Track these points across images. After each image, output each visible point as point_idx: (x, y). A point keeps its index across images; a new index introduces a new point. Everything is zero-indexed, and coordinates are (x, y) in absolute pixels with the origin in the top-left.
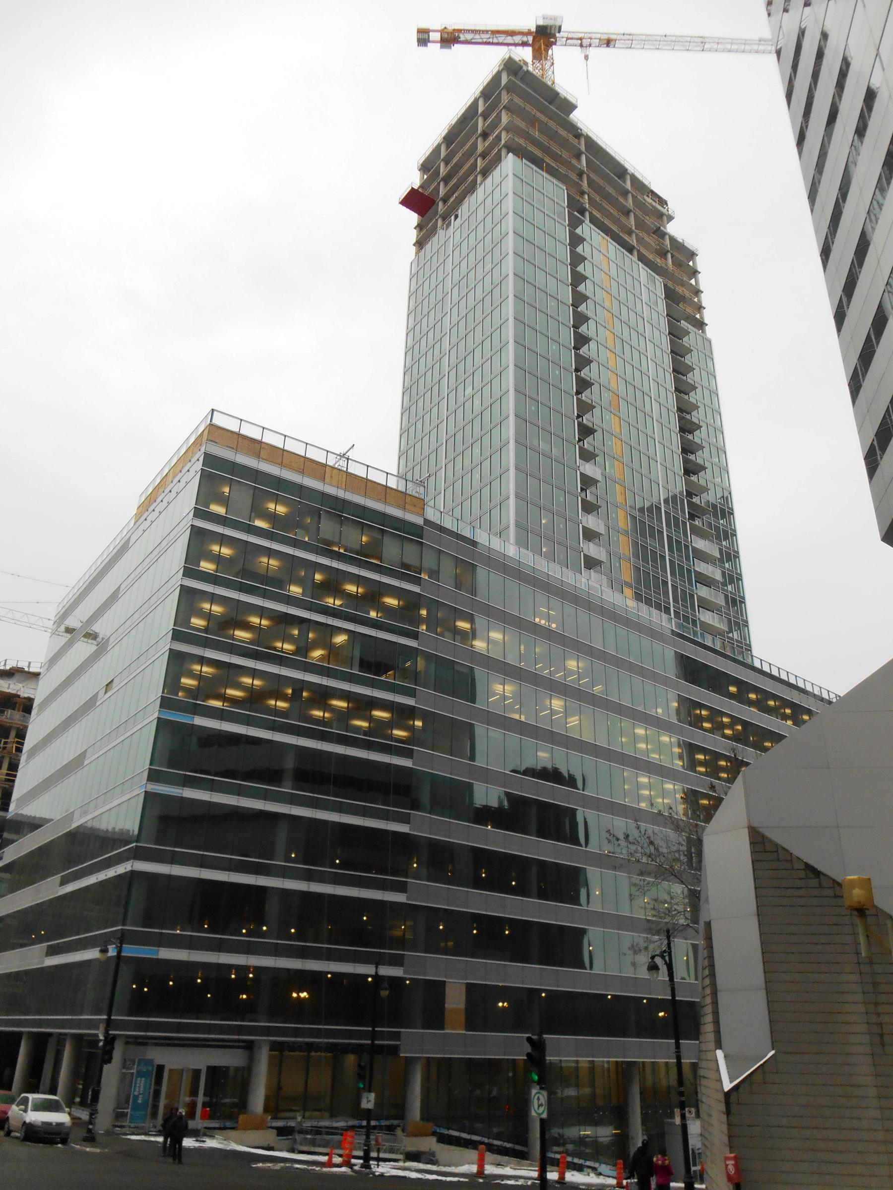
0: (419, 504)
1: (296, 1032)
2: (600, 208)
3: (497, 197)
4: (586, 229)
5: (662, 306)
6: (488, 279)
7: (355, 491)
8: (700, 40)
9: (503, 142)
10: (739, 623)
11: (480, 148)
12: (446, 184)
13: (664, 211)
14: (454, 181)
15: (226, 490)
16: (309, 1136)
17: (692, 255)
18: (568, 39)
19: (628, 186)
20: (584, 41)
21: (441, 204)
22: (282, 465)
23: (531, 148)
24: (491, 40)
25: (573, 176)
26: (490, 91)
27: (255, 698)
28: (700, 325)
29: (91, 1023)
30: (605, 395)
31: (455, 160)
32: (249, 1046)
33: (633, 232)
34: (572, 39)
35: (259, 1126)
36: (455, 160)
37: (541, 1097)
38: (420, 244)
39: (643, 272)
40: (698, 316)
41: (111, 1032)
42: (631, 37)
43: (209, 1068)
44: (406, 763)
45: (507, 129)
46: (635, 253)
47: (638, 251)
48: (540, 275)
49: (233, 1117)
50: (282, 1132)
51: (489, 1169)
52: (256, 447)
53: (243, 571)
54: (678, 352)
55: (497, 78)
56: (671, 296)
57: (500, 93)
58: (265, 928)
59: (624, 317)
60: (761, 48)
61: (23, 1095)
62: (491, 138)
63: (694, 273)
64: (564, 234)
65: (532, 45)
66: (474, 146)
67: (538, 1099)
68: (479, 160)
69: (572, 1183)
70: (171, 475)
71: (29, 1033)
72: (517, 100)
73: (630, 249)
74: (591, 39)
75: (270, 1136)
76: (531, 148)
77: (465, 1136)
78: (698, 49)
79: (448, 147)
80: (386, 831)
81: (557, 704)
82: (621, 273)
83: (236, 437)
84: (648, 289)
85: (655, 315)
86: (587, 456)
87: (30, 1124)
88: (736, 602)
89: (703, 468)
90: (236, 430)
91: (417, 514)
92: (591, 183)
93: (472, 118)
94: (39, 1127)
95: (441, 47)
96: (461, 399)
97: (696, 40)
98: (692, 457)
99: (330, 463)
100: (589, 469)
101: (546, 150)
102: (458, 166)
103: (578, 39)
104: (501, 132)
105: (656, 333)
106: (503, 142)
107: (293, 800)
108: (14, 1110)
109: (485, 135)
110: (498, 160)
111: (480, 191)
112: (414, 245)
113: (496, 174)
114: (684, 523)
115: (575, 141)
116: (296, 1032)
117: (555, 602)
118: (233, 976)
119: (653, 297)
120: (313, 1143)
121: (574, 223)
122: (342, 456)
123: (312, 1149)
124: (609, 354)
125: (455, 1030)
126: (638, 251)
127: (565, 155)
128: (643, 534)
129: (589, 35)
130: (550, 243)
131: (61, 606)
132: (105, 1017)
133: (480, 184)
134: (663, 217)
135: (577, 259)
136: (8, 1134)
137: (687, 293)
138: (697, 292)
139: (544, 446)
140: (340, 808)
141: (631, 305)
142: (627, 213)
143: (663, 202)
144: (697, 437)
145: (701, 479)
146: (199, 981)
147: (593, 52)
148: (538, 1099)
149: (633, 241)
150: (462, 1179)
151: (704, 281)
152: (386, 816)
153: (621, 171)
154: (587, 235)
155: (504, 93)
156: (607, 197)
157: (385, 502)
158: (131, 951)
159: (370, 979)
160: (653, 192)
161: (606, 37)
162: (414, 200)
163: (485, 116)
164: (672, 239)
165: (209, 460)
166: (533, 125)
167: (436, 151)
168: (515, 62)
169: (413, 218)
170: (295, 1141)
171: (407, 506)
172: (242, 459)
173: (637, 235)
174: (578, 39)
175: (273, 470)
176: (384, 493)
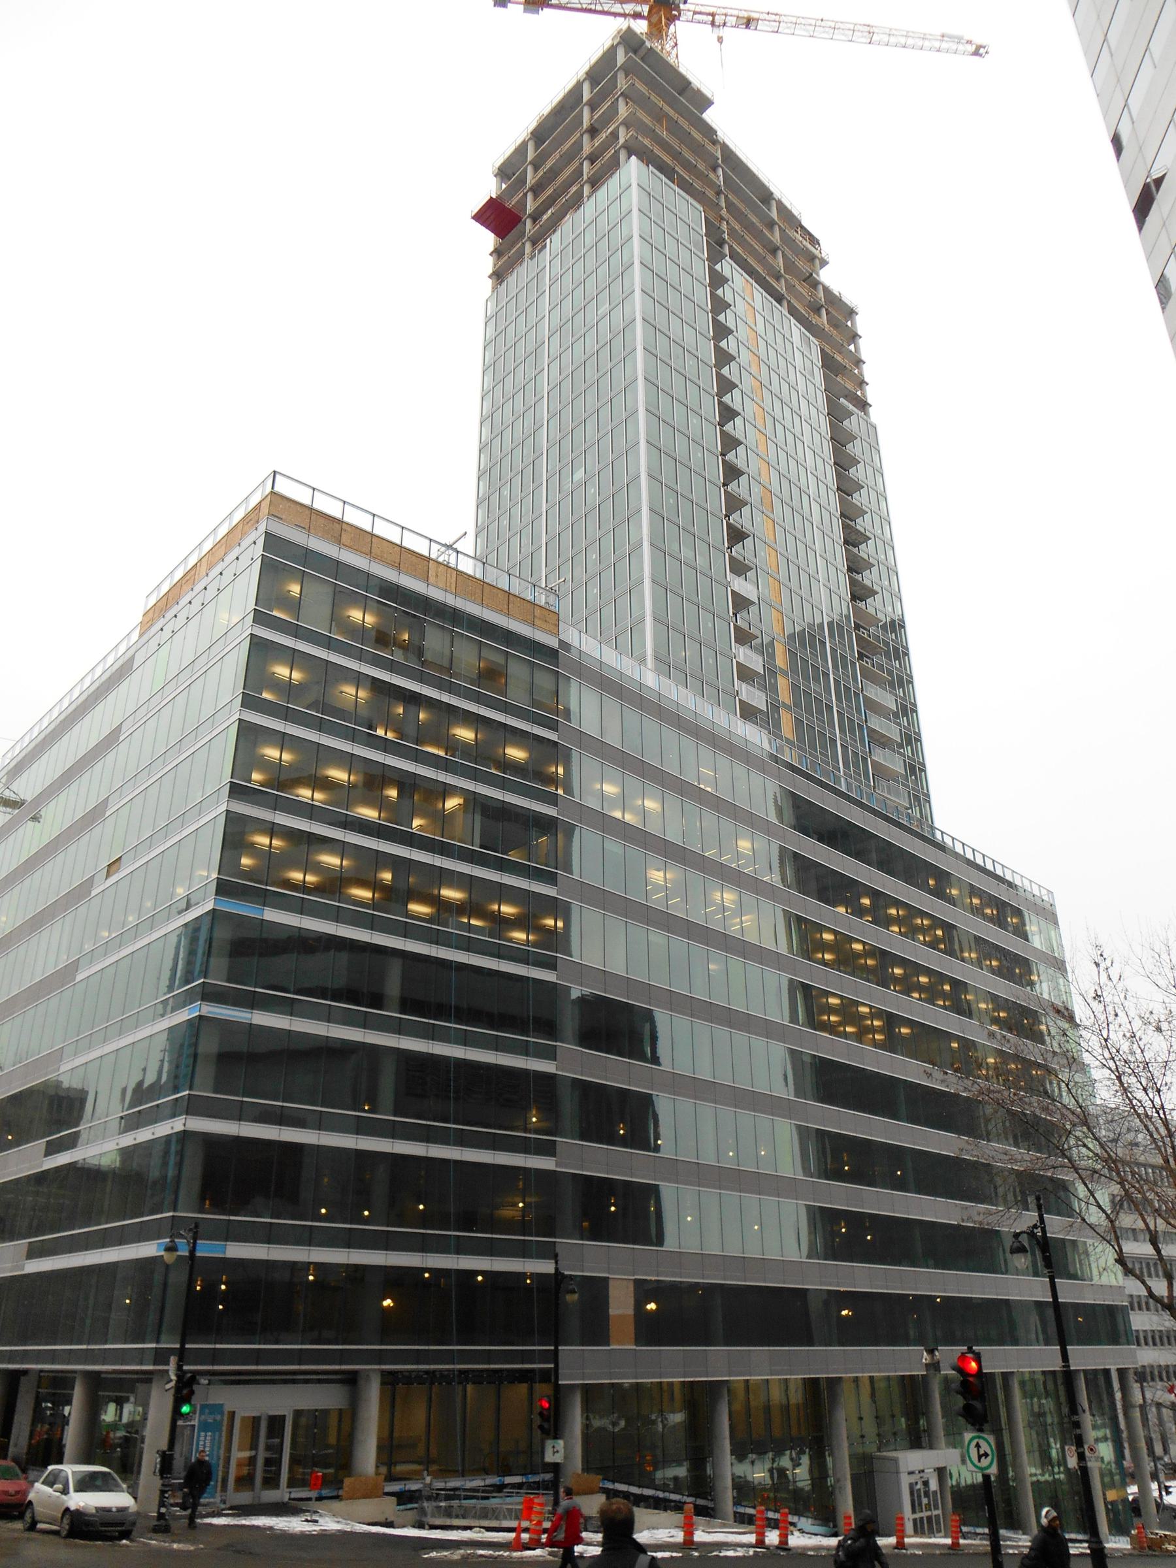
0: (551, 618)
1: (418, 1357)
2: (742, 242)
3: (615, 212)
4: (726, 267)
5: (818, 377)
6: (604, 325)
7: (469, 596)
8: (867, 29)
9: (622, 141)
10: (921, 798)
11: (587, 149)
12: (536, 197)
13: (816, 253)
14: (549, 191)
15: (295, 589)
16: (443, 1504)
17: (851, 313)
18: (695, 13)
19: (774, 214)
20: (717, 17)
21: (529, 222)
22: (370, 555)
23: (658, 151)
24: (593, 7)
25: (710, 193)
26: (600, 73)
27: (334, 884)
28: (863, 405)
29: (119, 1353)
30: (756, 489)
31: (549, 164)
32: (351, 1380)
33: (781, 276)
34: (700, 13)
35: (370, 1493)
36: (549, 164)
37: (982, 1443)
38: (498, 276)
39: (796, 331)
40: (859, 393)
41: (185, 1368)
42: (777, 18)
43: (298, 1414)
44: (548, 976)
45: (626, 124)
46: (785, 304)
47: (789, 302)
48: (675, 323)
49: (337, 1483)
50: (403, 1498)
51: (700, 1536)
52: (335, 527)
53: (314, 701)
54: (840, 440)
55: (609, 56)
56: (829, 365)
57: (615, 76)
58: (366, 1213)
59: (775, 387)
60: (944, 45)
61: (50, 1468)
62: (604, 135)
63: (854, 337)
64: (701, 270)
65: (648, 18)
66: (579, 145)
67: (978, 1446)
68: (586, 164)
69: (798, 1548)
70: (203, 568)
71: (87, 1374)
72: (640, 86)
73: (779, 299)
74: (726, 15)
75: (389, 1507)
76: (658, 151)
77: (634, 1490)
78: (864, 40)
79: (537, 146)
80: (526, 1072)
81: (730, 897)
82: (770, 329)
83: (308, 512)
84: (800, 353)
85: (811, 387)
86: (739, 568)
87: (77, 1511)
88: (916, 769)
89: (873, 593)
90: (307, 502)
91: (550, 633)
92: (730, 206)
93: (573, 108)
94: (92, 1515)
95: (525, 11)
96: (568, 487)
97: (861, 28)
98: (859, 577)
99: (433, 556)
100: (740, 585)
101: (677, 156)
102: (553, 174)
103: (709, 14)
104: (618, 127)
105: (813, 411)
106: (622, 141)
107: (400, 1029)
108: (40, 1492)
109: (593, 131)
110: (614, 165)
111: (589, 208)
112: (490, 277)
113: (613, 184)
114: (853, 664)
115: (710, 147)
116: (418, 1357)
117: (724, 761)
118: (311, 1278)
119: (808, 363)
120: (448, 1512)
121: (715, 257)
122: (449, 547)
123: (448, 1522)
124: (759, 436)
125: (623, 1344)
126: (789, 302)
127: (701, 166)
128: (806, 677)
129: (724, 11)
130: (686, 283)
131: (9, 756)
132: (178, 1346)
133: (589, 197)
134: (815, 261)
135: (720, 305)
136: (32, 1527)
137: (846, 363)
138: (859, 362)
139: (686, 553)
140: (465, 1040)
141: (783, 374)
142: (774, 251)
143: (814, 241)
144: (865, 551)
145: (872, 606)
146: (223, 1287)
147: (726, 32)
148: (978, 1446)
149: (781, 287)
150: (674, 1554)
151: (866, 348)
152: (525, 1050)
153: (766, 196)
154: (727, 272)
155: (621, 76)
156: (749, 226)
157: (508, 615)
158: (207, 1249)
159: (480, 1278)
160: (802, 227)
161: (746, 15)
162: (497, 217)
163: (593, 106)
164: (826, 290)
165: (272, 541)
166: (659, 121)
167: (521, 150)
168: (635, 34)
169: (487, 239)
170: (423, 1512)
171: (537, 622)
172: (317, 544)
173: (786, 281)
174: (709, 14)
175: (359, 561)
176: (506, 602)
